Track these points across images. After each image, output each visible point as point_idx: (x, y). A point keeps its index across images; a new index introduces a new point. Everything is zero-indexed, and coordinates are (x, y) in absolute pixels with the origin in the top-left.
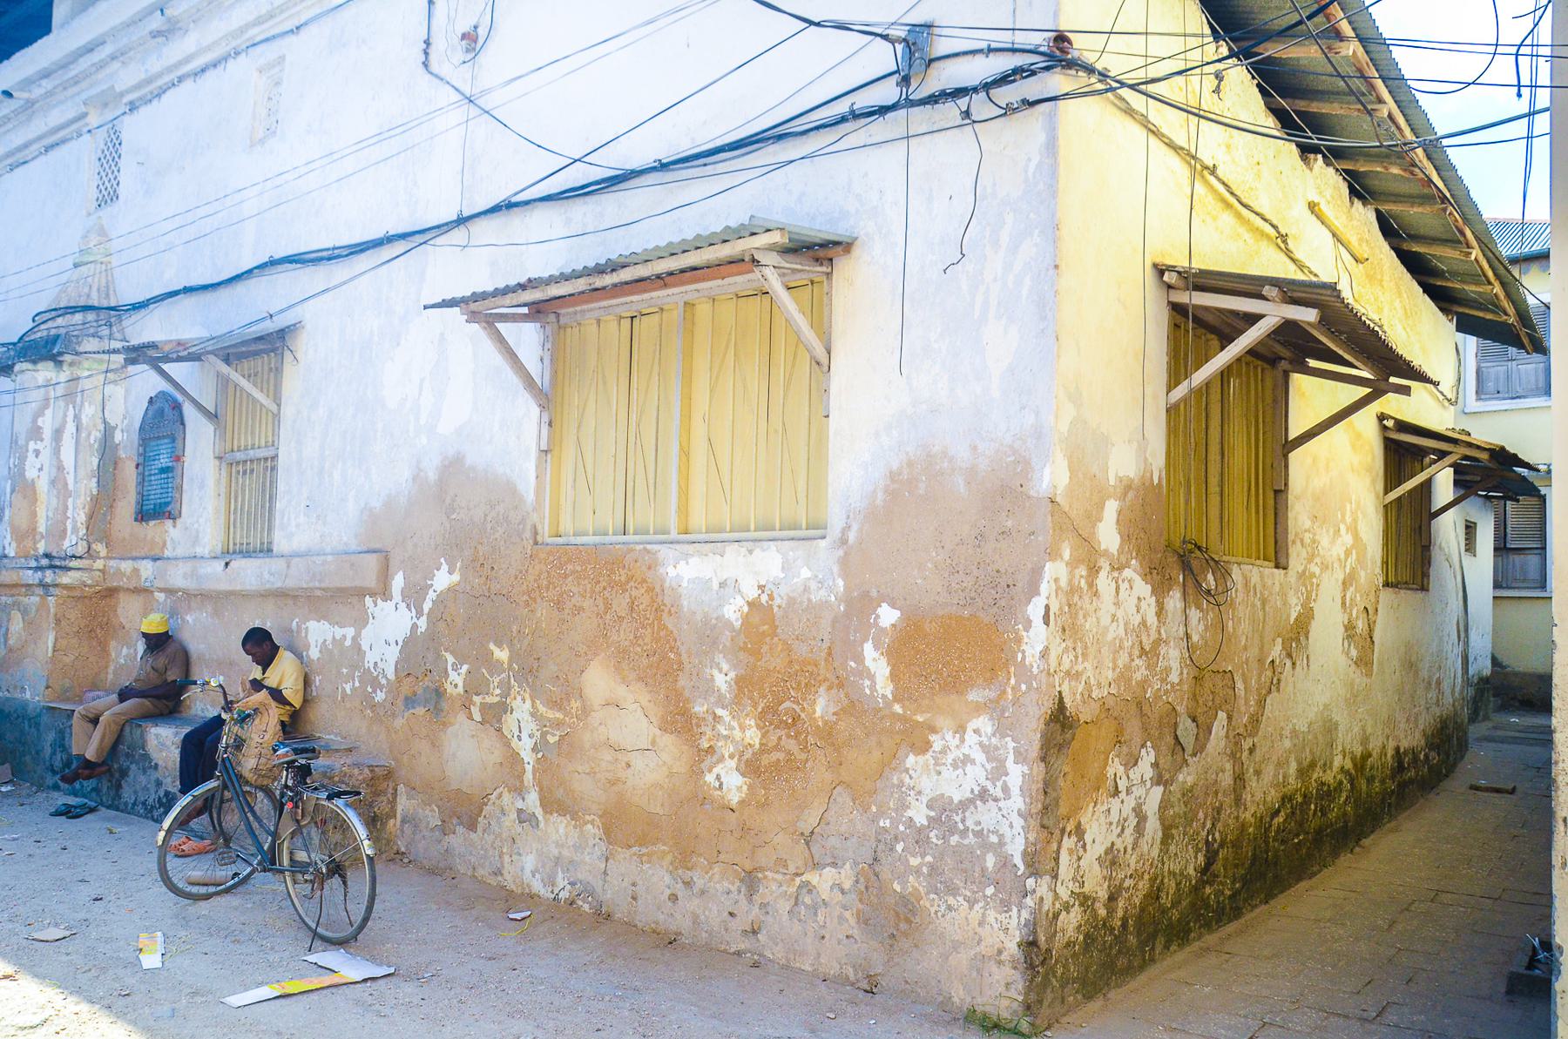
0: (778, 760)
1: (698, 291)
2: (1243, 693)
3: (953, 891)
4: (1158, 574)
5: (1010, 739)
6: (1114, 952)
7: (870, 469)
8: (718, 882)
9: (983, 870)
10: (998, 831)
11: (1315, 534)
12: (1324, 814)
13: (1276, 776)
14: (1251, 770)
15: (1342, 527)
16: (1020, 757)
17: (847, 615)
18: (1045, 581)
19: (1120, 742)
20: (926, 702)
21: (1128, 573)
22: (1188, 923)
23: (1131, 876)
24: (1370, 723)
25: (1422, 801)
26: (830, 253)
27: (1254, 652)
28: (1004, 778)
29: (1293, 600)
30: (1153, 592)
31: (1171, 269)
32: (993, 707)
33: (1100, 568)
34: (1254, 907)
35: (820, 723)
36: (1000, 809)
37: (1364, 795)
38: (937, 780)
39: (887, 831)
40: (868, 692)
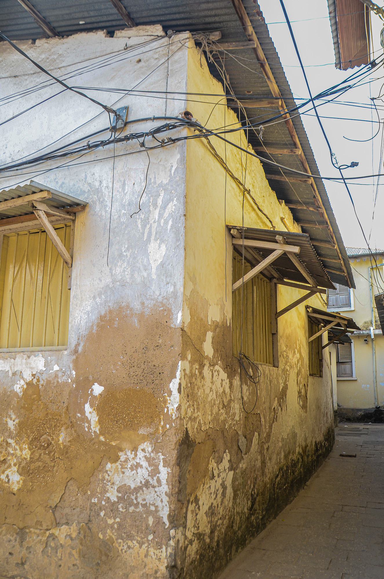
0: (39, 466)
1: (11, 229)
2: (264, 423)
3: (130, 537)
4: (230, 368)
5: (160, 454)
6: (214, 560)
7: (90, 315)
8: (5, 535)
9: (147, 526)
10: (155, 504)
11: (287, 353)
12: (294, 474)
13: (277, 459)
14: (268, 458)
15: (296, 350)
16: (166, 464)
17: (77, 389)
18: (179, 370)
19: (214, 451)
20: (117, 435)
21: (217, 367)
22: (245, 536)
23: (220, 519)
24: (307, 432)
25: (324, 462)
26: (75, 209)
27: (267, 405)
28: (157, 475)
29: (281, 381)
30: (228, 377)
31: (234, 227)
32: (151, 437)
33: (205, 365)
34: (270, 522)
35: (62, 447)
36: (156, 492)
37: (306, 463)
38: (123, 477)
39: (95, 504)
40: (87, 429)
